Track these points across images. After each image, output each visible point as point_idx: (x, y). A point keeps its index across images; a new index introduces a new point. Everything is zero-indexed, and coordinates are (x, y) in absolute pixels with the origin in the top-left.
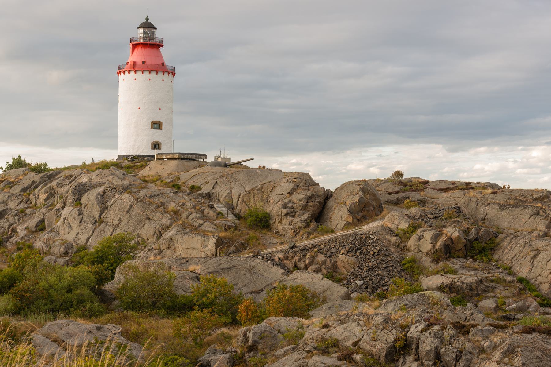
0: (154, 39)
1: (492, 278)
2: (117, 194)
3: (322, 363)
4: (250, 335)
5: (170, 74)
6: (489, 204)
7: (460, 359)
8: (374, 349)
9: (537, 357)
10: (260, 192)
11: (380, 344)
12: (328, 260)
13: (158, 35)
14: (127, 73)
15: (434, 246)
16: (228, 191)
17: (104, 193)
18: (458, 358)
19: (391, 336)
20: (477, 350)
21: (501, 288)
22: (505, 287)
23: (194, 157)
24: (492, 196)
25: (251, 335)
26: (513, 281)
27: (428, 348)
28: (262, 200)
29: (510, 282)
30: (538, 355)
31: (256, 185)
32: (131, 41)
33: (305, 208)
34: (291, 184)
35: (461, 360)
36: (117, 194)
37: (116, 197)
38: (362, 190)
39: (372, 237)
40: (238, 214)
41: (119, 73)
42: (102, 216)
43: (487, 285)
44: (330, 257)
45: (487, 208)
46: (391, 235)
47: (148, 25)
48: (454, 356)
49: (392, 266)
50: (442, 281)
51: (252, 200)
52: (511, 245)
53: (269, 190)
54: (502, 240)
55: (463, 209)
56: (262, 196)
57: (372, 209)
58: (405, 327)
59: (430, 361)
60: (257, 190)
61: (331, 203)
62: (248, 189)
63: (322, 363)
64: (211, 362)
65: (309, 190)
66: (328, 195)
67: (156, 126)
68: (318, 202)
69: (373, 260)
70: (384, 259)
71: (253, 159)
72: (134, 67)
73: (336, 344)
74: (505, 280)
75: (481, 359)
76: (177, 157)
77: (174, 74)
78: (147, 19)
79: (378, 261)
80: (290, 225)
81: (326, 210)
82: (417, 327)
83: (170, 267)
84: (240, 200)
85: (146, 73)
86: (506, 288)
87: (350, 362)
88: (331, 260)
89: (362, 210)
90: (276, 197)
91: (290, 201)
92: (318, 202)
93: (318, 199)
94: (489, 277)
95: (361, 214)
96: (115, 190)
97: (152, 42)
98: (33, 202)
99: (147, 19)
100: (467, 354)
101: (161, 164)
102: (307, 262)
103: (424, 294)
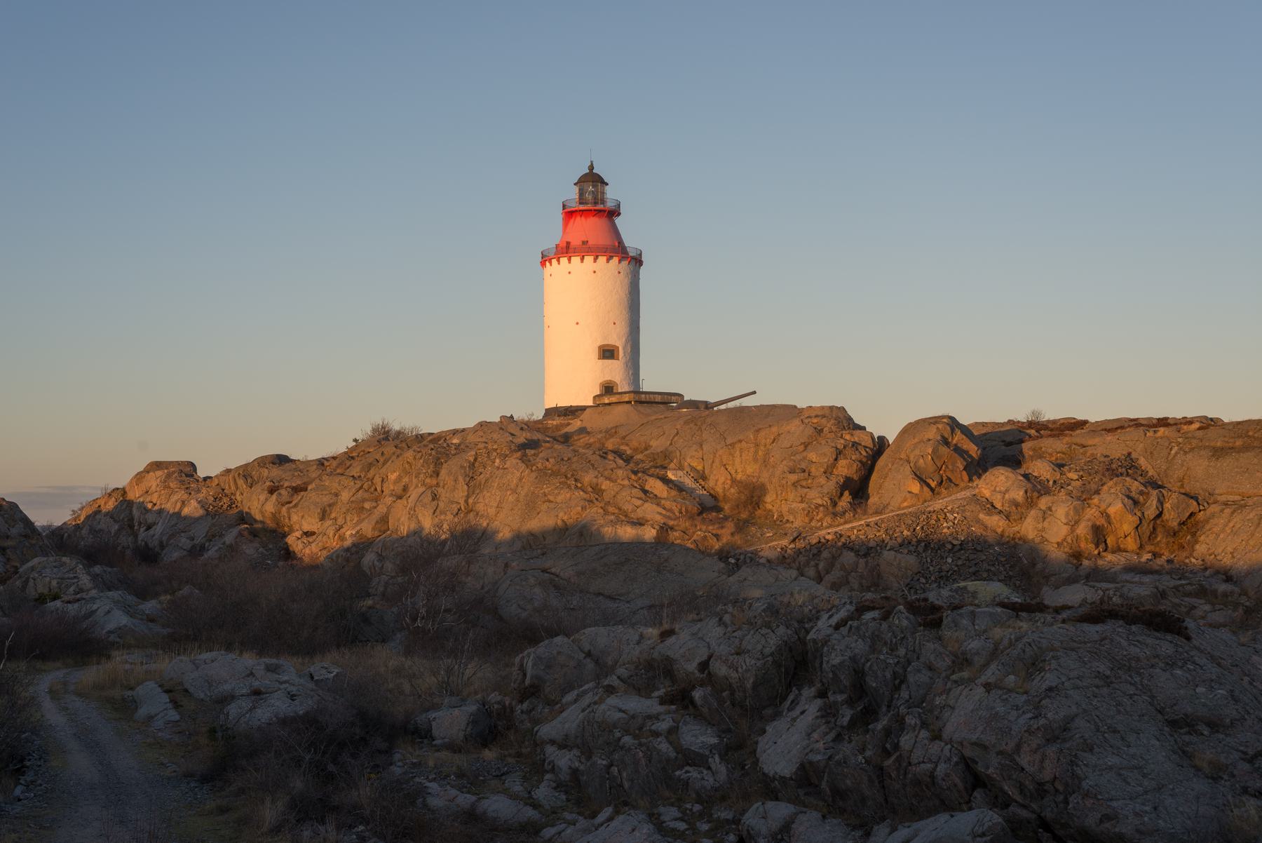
0: (603, 201)
1: (1189, 588)
3: (620, 710)
4: (529, 664)
6: (1192, 449)
7: (902, 682)
8: (735, 675)
9: (1098, 675)
11: (748, 660)
12: (862, 561)
13: (612, 194)
14: (554, 261)
15: (1073, 531)
18: (897, 682)
19: (772, 641)
20: (948, 661)
21: (1207, 607)
22: (1213, 604)
24: (1201, 433)
25: (530, 664)
26: (1232, 593)
27: (836, 661)
28: (755, 460)
29: (1225, 595)
30: (1102, 668)
32: (564, 206)
35: (904, 686)
39: (950, 517)
41: (543, 264)
42: (470, 501)
43: (1177, 601)
44: (865, 555)
45: (1189, 456)
46: (989, 514)
47: (592, 180)
48: (888, 675)
49: (988, 571)
50: (1083, 596)
51: (737, 460)
52: (1231, 525)
54: (1213, 516)
55: (1142, 462)
58: (806, 621)
59: (841, 692)
63: (620, 710)
64: (434, 724)
69: (949, 560)
70: (972, 557)
72: (565, 250)
73: (666, 668)
74: (1214, 593)
75: (956, 682)
78: (591, 168)
79: (960, 563)
80: (802, 502)
82: (830, 617)
83: (507, 565)
85: (589, 259)
86: (1218, 607)
87: (686, 708)
88: (867, 563)
91: (805, 458)
94: (1182, 585)
97: (601, 207)
98: (379, 489)
99: (591, 168)
100: (919, 671)
102: (821, 566)
103: (965, 588)
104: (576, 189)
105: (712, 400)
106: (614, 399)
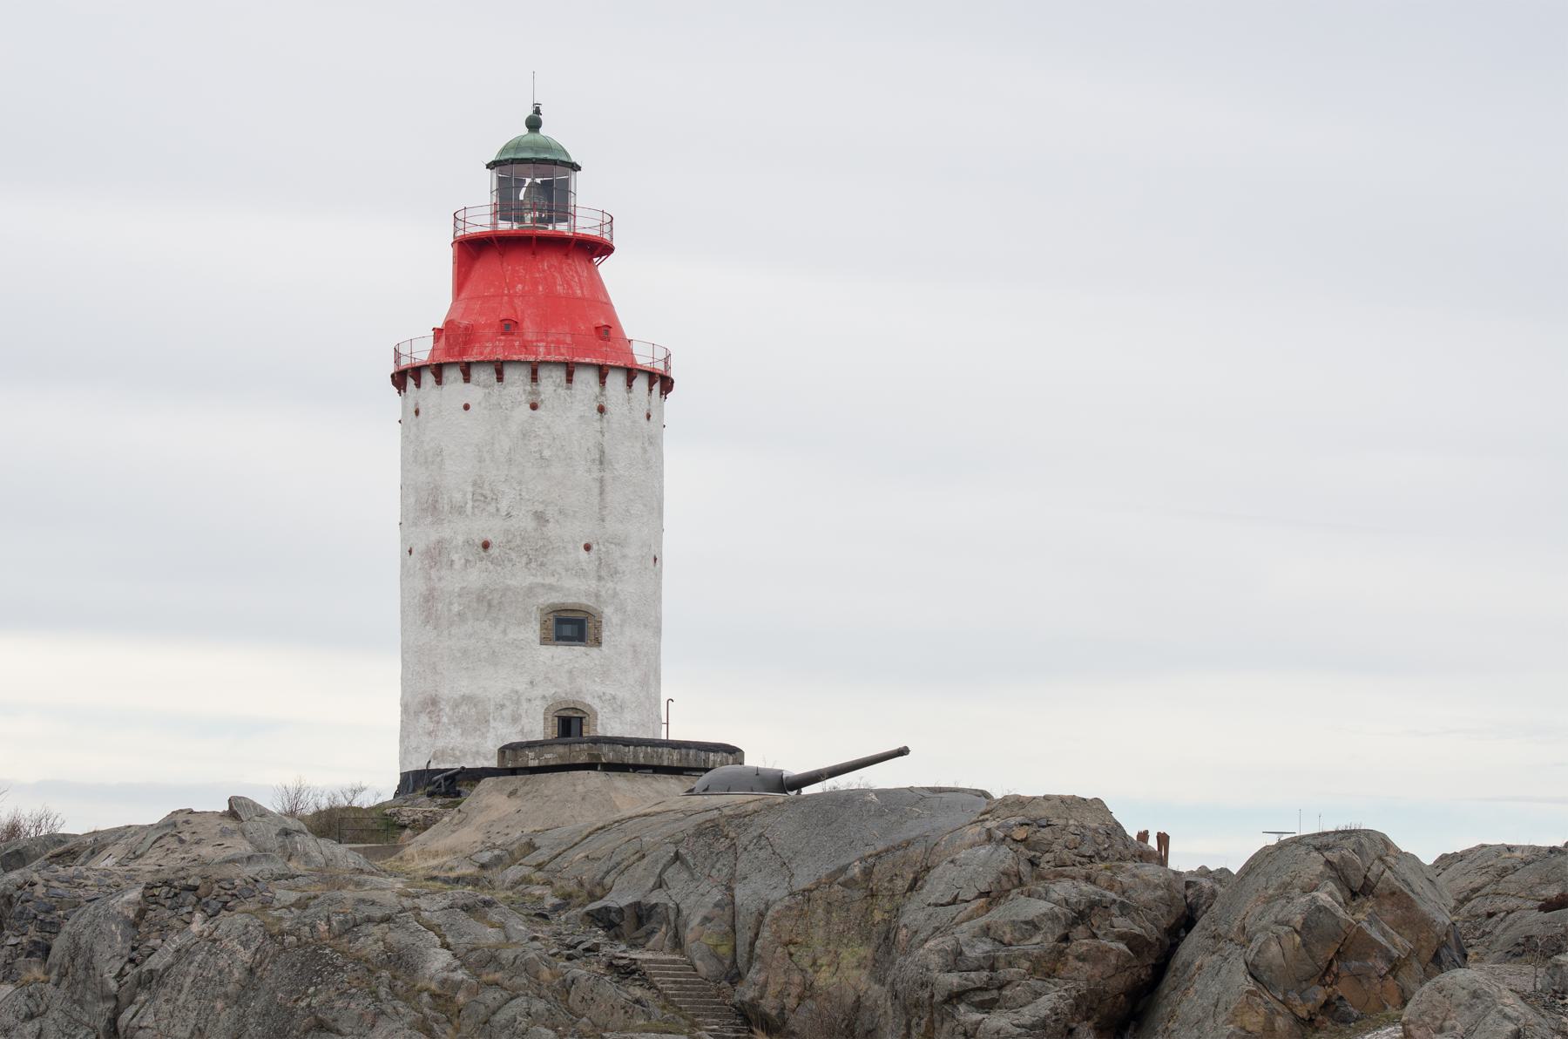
2: (198, 916)
5: (641, 383)
10: (858, 894)
16: (717, 895)
17: (141, 914)
23: (693, 758)
31: (843, 862)
33: (1047, 968)
34: (1004, 849)
36: (198, 916)
37: (196, 927)
38: (1338, 872)
40: (753, 1004)
53: (901, 884)
56: (868, 912)
57: (1382, 966)
60: (844, 884)
61: (1193, 942)
62: (802, 881)
65: (1088, 878)
66: (1190, 907)
67: (567, 630)
68: (1121, 937)
71: (903, 752)
76: (583, 759)
77: (666, 384)
78: (534, 124)
81: (1169, 980)
84: (766, 933)
89: (1325, 974)
90: (921, 916)
91: (986, 931)
92: (1121, 937)
93: (1122, 924)
95: (1320, 995)
96: (192, 898)
99: (534, 124)
101: (512, 794)
104: (489, 180)
105: (794, 767)
106: (581, 754)
